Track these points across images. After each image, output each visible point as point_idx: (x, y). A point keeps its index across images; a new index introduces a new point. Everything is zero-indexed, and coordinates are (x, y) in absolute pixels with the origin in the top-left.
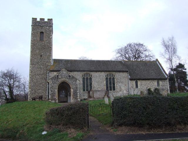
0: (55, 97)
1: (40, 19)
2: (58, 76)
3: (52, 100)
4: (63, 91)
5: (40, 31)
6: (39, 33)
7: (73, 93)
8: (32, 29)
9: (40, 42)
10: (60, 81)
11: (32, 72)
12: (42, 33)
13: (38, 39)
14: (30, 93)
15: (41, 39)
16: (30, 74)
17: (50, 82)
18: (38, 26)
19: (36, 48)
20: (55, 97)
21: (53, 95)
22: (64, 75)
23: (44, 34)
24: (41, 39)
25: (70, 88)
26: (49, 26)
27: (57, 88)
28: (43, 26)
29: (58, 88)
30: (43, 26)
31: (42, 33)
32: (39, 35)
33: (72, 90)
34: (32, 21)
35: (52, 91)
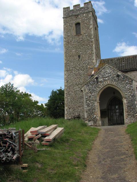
0: (95, 116)
1: (74, 6)
2: (97, 78)
3: (89, 121)
4: (117, 107)
5: (75, 22)
6: (74, 25)
7: (128, 106)
8: (64, 23)
9: (76, 37)
10: (101, 86)
11: (67, 82)
12: (78, 24)
13: (74, 33)
14: (66, 113)
15: (78, 33)
16: (65, 85)
17: (85, 90)
18: (71, 16)
19: (71, 46)
20: (95, 116)
21: (91, 112)
22: (107, 75)
23: (81, 25)
24: (78, 33)
25: (122, 97)
26: (86, 13)
27: (98, 98)
28: (77, 15)
29: (100, 100)
30: (77, 15)
31: (78, 24)
32: (75, 28)
33: (125, 101)
34: (64, 12)
35: (88, 105)
